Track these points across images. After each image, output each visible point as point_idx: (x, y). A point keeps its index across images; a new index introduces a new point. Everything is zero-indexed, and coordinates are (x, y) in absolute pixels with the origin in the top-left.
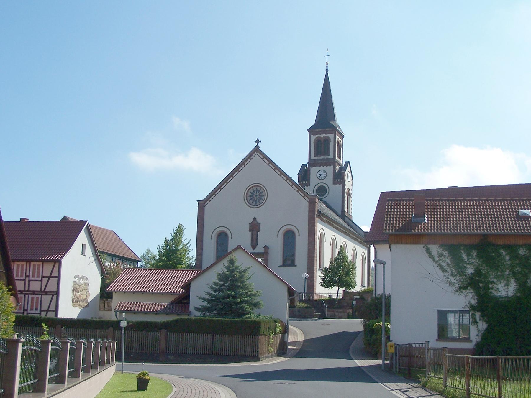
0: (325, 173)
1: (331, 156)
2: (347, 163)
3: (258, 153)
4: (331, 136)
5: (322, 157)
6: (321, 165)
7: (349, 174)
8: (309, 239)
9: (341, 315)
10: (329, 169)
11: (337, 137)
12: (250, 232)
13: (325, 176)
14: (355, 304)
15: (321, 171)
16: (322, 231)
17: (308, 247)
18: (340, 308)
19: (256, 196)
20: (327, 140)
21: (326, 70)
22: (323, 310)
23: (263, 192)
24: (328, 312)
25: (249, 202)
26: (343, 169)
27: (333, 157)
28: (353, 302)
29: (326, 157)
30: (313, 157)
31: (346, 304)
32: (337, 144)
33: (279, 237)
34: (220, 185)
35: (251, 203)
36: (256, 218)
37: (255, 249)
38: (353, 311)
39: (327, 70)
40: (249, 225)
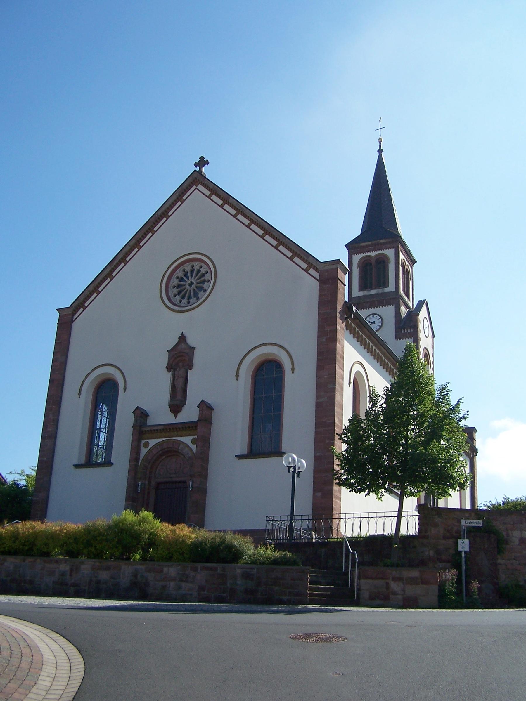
0: (380, 320)
1: (391, 288)
2: (421, 303)
3: (200, 187)
4: (390, 253)
5: (373, 292)
6: (372, 305)
7: (427, 323)
8: (318, 377)
9: (412, 590)
10: (388, 312)
11: (402, 256)
12: (169, 371)
13: (380, 324)
14: (467, 549)
15: (371, 316)
16: (357, 368)
17: (318, 397)
18: (411, 565)
19: (191, 284)
20: (383, 262)
21: (378, 151)
22: (346, 574)
23: (207, 272)
24: (362, 581)
25: (172, 300)
26: (413, 315)
27: (394, 290)
28: (459, 541)
29: (380, 291)
30: (356, 293)
31: (432, 553)
32: (401, 268)
33: (240, 378)
34: (108, 270)
35: (177, 303)
36: (186, 334)
37: (179, 415)
38: (459, 575)
39: (380, 151)
40: (167, 355)
